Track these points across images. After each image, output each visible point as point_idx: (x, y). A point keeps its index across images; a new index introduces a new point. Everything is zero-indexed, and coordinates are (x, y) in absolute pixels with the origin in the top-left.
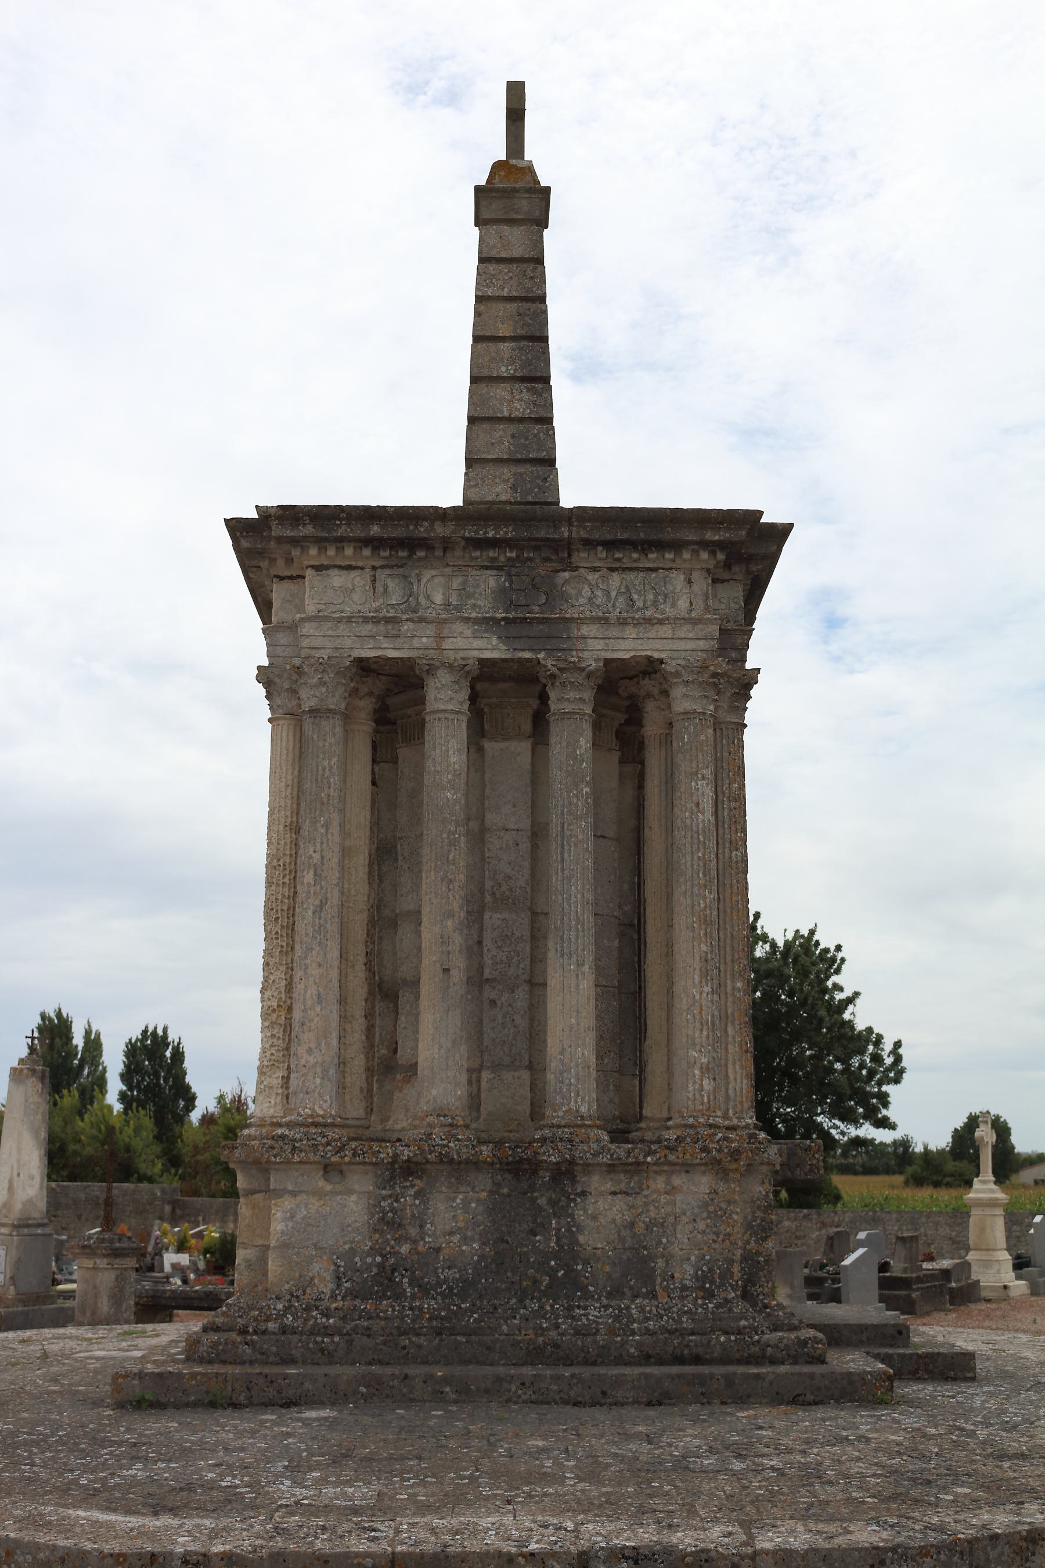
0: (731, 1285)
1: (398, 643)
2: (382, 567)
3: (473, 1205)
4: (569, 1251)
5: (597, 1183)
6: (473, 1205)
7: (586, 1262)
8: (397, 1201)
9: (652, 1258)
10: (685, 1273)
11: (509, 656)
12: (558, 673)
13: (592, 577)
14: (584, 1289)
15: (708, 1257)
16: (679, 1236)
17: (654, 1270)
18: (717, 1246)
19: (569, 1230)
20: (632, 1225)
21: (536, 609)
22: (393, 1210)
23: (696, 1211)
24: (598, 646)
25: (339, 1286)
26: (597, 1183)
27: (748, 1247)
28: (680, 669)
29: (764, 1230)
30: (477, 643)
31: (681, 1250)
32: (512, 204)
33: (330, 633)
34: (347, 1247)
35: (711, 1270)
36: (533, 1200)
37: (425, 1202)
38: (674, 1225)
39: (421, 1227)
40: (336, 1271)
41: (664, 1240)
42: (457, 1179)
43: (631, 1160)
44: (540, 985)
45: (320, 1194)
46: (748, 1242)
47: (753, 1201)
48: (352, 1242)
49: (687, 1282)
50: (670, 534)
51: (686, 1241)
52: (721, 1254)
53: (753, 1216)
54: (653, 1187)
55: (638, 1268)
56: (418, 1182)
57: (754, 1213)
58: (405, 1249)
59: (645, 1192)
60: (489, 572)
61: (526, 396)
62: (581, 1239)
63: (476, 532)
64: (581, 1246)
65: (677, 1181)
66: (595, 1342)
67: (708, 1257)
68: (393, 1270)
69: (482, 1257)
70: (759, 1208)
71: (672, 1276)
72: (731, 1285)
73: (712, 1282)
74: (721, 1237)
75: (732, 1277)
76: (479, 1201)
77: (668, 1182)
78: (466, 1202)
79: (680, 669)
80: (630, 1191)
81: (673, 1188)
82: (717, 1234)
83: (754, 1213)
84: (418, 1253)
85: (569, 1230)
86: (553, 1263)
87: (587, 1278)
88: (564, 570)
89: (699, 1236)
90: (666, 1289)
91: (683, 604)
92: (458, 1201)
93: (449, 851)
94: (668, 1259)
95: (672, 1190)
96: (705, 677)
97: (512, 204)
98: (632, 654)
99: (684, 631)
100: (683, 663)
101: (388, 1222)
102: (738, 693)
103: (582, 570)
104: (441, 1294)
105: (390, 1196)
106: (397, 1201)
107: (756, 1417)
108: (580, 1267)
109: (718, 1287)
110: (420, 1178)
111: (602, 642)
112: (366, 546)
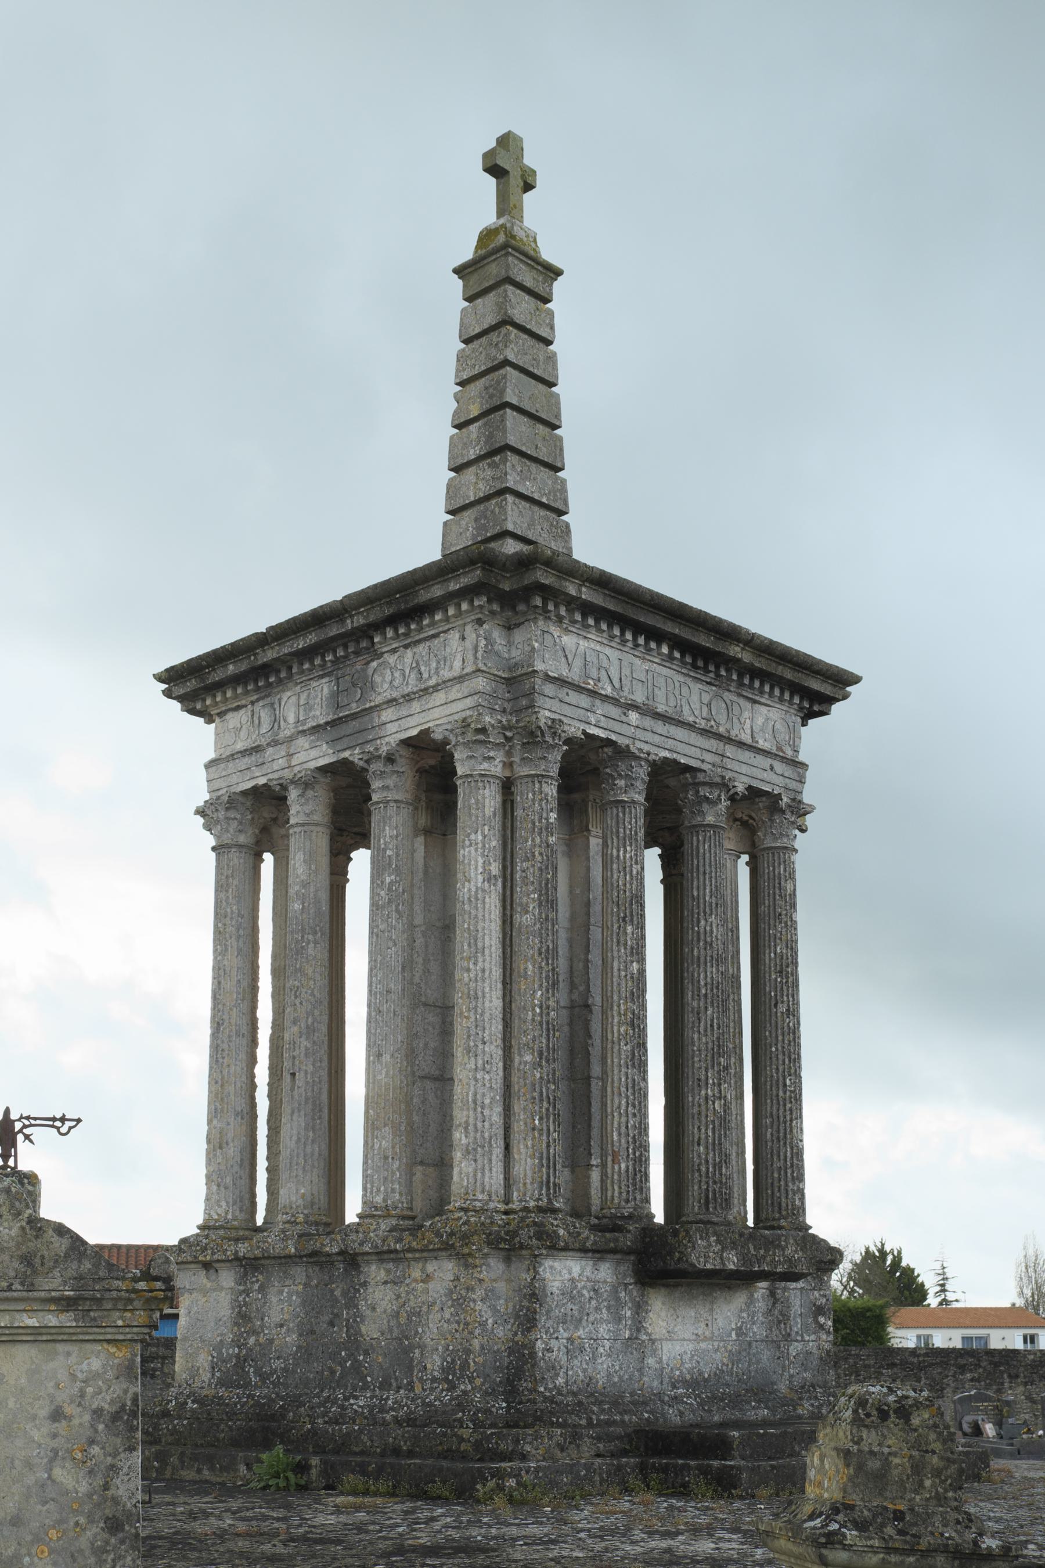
0: (468, 1377)
1: (265, 769)
2: (258, 700)
3: (294, 1298)
4: (354, 1342)
5: (375, 1272)
6: (294, 1298)
7: (366, 1353)
8: (248, 1295)
9: (412, 1348)
10: (434, 1363)
11: (335, 759)
12: (365, 766)
13: (391, 659)
14: (363, 1378)
15: (451, 1348)
16: (431, 1325)
17: (412, 1359)
18: (457, 1335)
19: (355, 1321)
20: (397, 1314)
21: (354, 705)
22: (246, 1304)
23: (444, 1299)
24: (396, 728)
25: (213, 1375)
26: (375, 1272)
27: (516, 1339)
28: (447, 733)
29: (528, 1321)
30: (314, 753)
31: (432, 1339)
32: (506, 275)
33: (224, 773)
34: (218, 1339)
35: (453, 1361)
36: (332, 1291)
37: (264, 1296)
38: (428, 1312)
39: (262, 1319)
40: (212, 1361)
41: (420, 1330)
42: (285, 1273)
43: (385, 1248)
44: (449, 1079)
45: (205, 1292)
46: (516, 1334)
47: (520, 1290)
48: (222, 1335)
49: (436, 1373)
50: (426, 595)
51: (435, 1331)
52: (461, 1344)
53: (521, 1306)
54: (413, 1275)
55: (404, 1350)
56: (260, 1277)
57: (521, 1302)
58: (252, 1341)
59: (407, 1281)
60: (324, 680)
61: (489, 472)
62: (363, 1329)
63: (292, 647)
64: (362, 1336)
65: (430, 1267)
66: (341, 1430)
67: (451, 1348)
68: (245, 1360)
69: (299, 1347)
70: (525, 1295)
71: (425, 1368)
72: (468, 1377)
73: (454, 1375)
74: (462, 1326)
75: (469, 1367)
76: (297, 1293)
77: (423, 1270)
78: (290, 1295)
79: (447, 733)
80: (396, 1280)
81: (428, 1276)
82: (458, 1323)
83: (521, 1302)
84: (260, 1345)
85: (355, 1321)
86: (343, 1353)
87: (366, 1368)
88: (372, 660)
89: (446, 1325)
90: (421, 1380)
91: (457, 664)
92: (285, 1294)
93: (296, 960)
94: (422, 1347)
95: (427, 1278)
96: (470, 736)
97: (506, 275)
98: (419, 729)
99: (455, 692)
100: (449, 727)
101: (243, 1316)
102: (528, 743)
103: (386, 655)
104: (272, 1383)
105: (244, 1291)
106: (248, 1295)
107: (413, 1511)
108: (361, 1358)
109: (458, 1379)
110: (261, 1273)
111: (396, 724)
112: (239, 684)
